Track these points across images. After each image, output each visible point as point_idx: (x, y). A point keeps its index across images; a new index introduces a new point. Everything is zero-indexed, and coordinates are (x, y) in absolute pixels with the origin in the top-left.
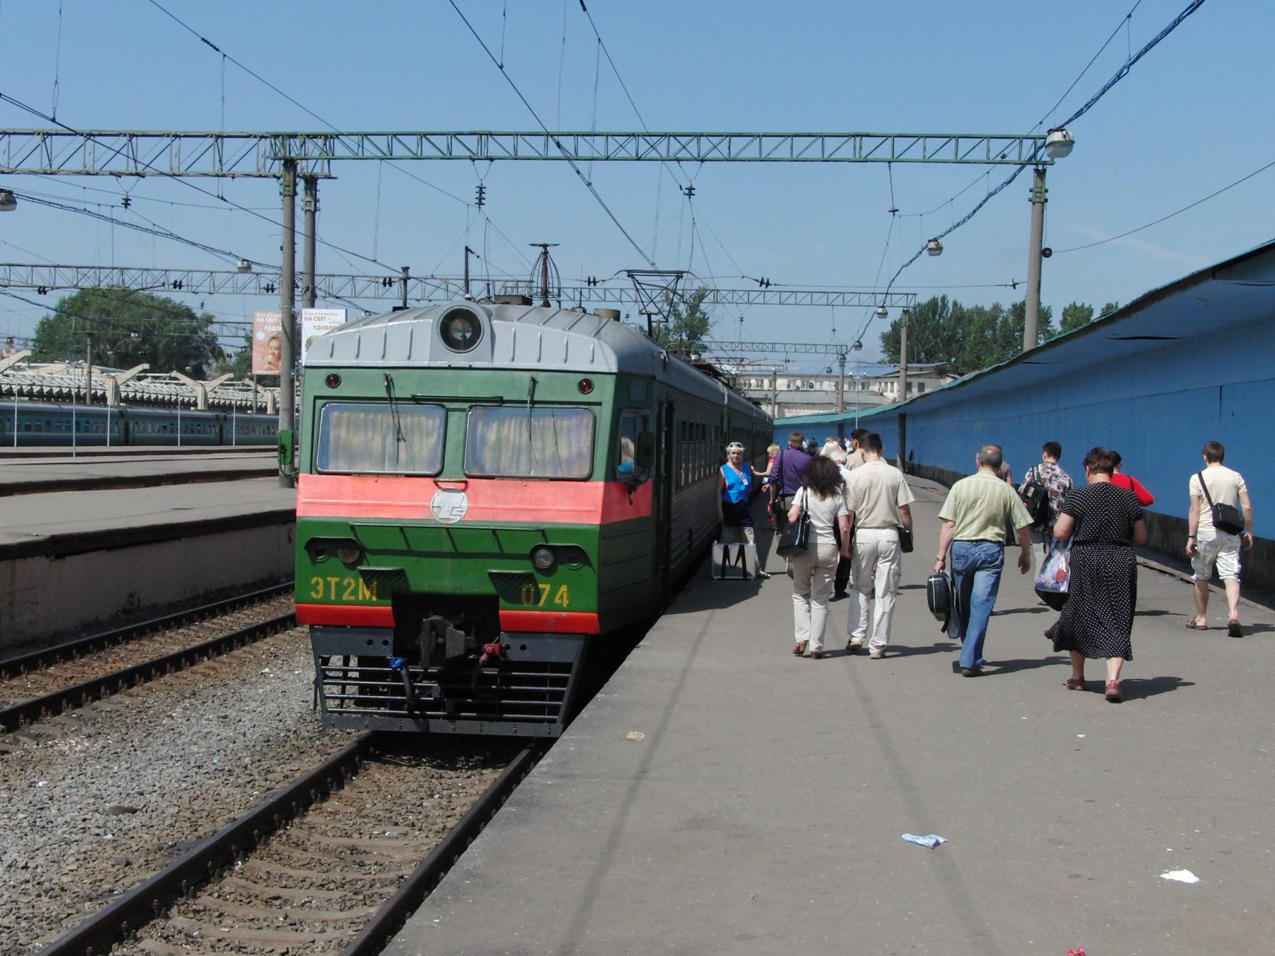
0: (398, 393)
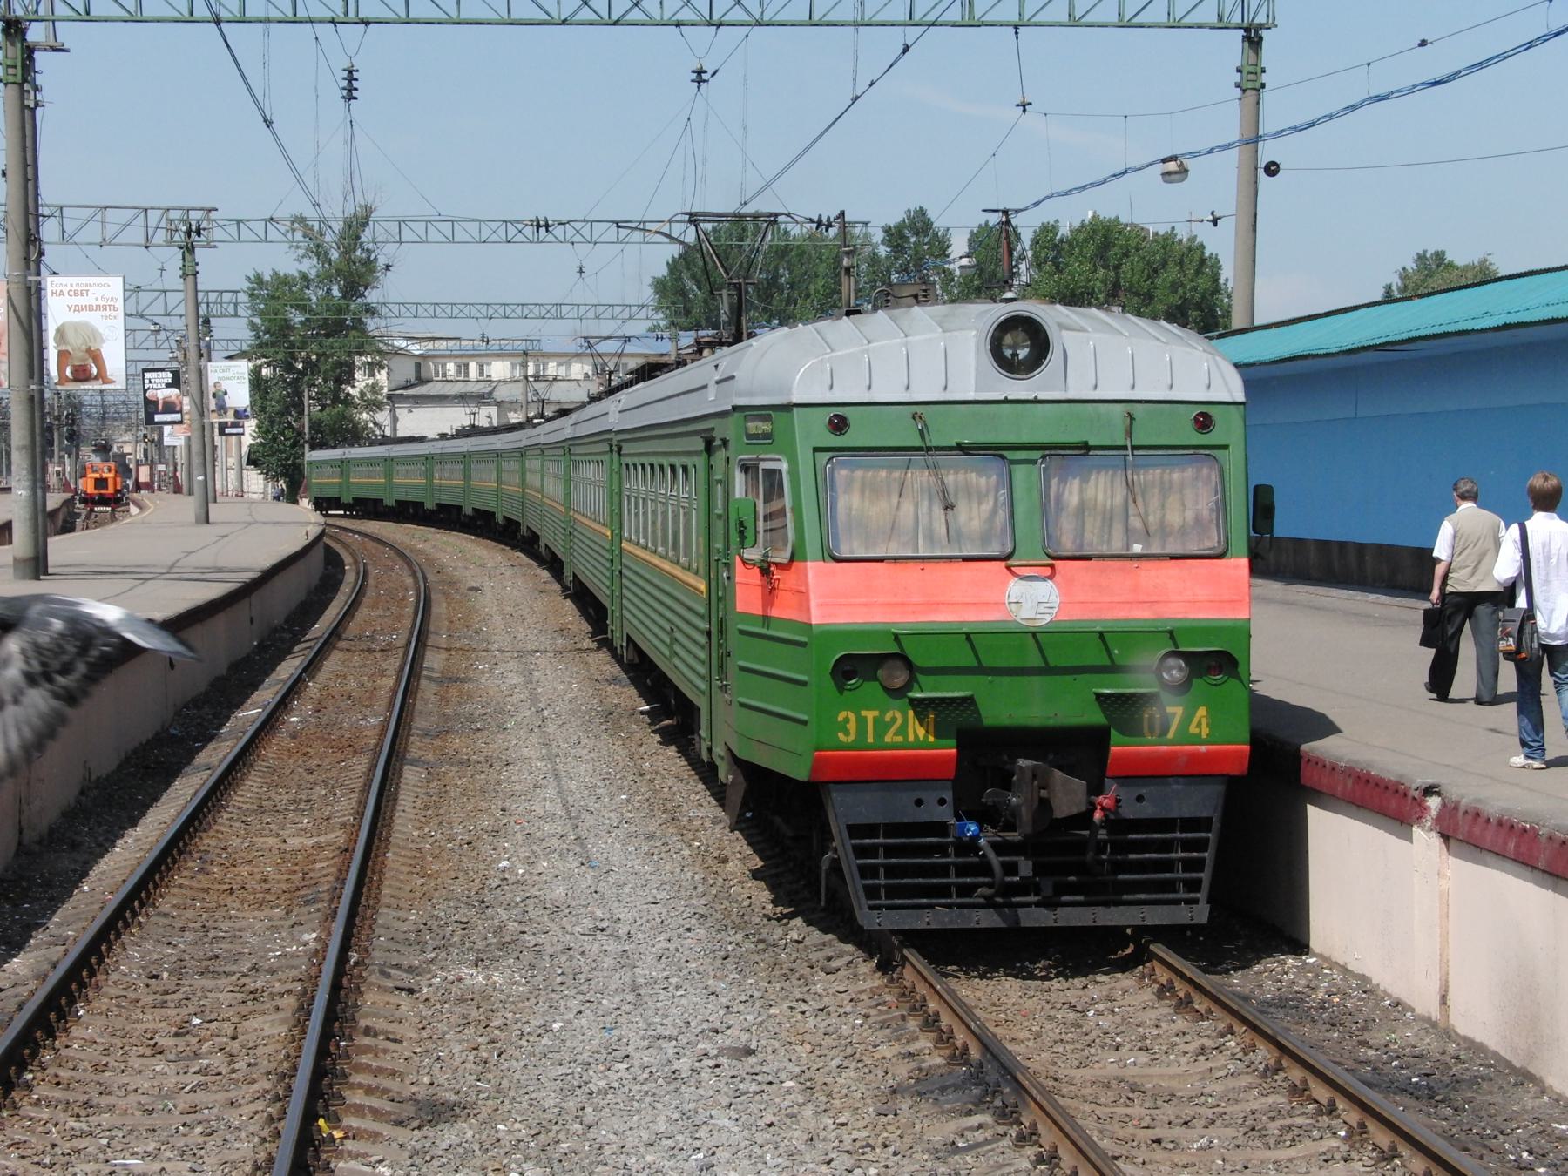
0: (934, 440)
